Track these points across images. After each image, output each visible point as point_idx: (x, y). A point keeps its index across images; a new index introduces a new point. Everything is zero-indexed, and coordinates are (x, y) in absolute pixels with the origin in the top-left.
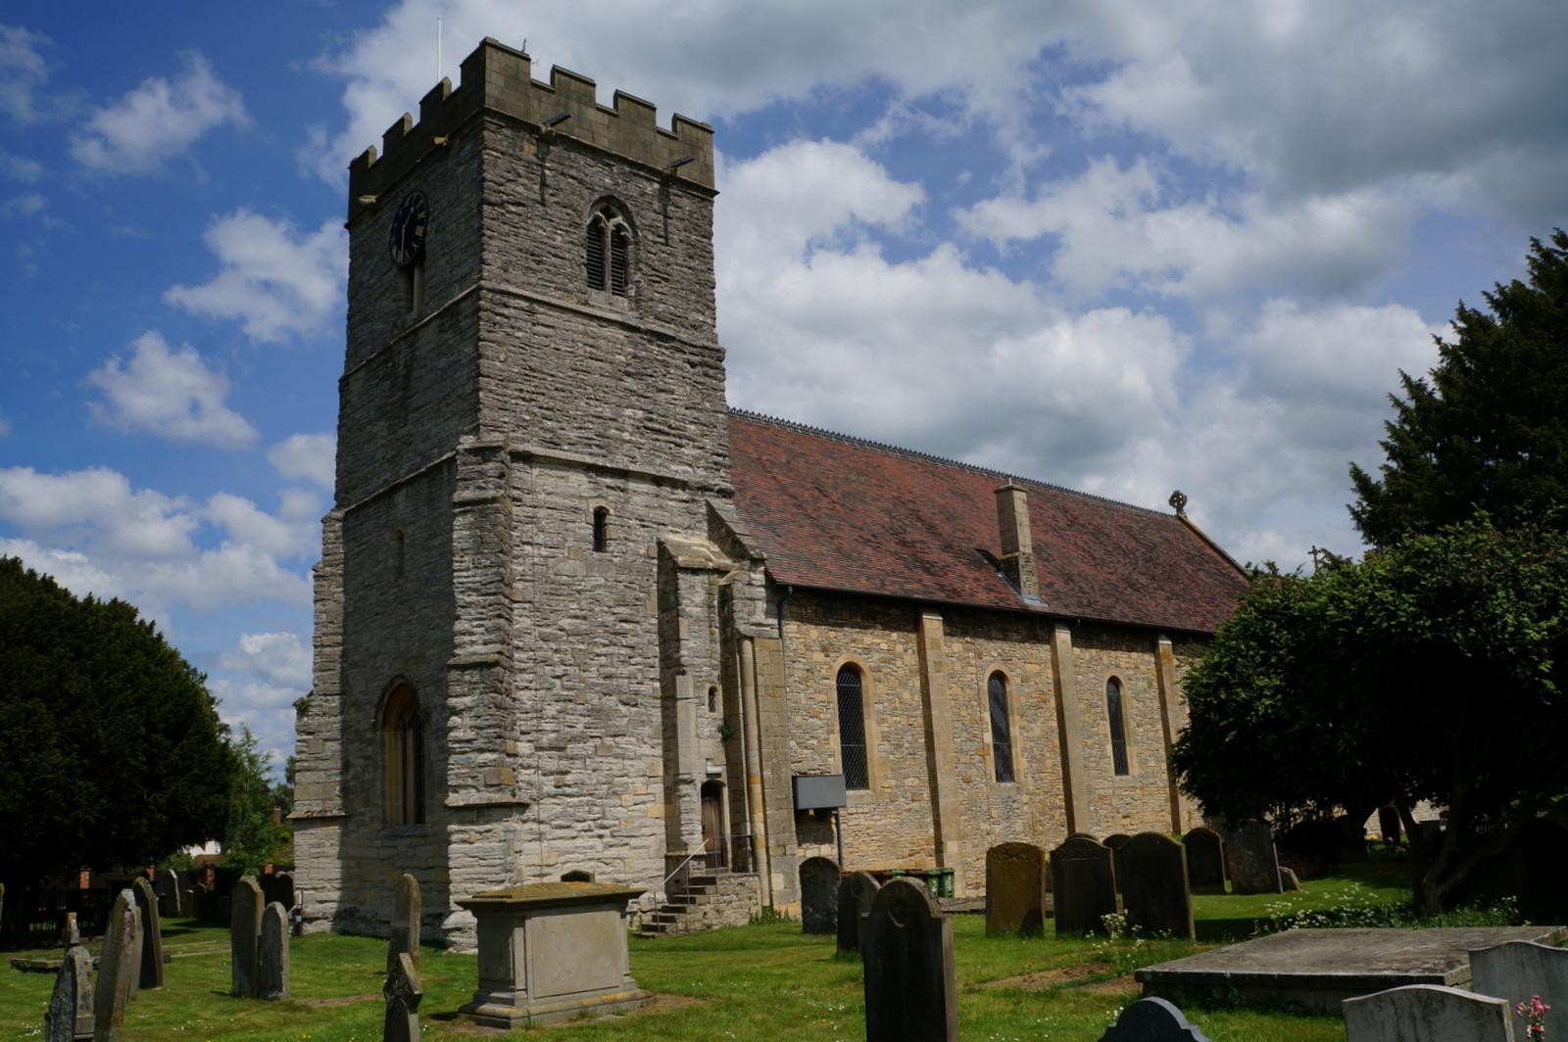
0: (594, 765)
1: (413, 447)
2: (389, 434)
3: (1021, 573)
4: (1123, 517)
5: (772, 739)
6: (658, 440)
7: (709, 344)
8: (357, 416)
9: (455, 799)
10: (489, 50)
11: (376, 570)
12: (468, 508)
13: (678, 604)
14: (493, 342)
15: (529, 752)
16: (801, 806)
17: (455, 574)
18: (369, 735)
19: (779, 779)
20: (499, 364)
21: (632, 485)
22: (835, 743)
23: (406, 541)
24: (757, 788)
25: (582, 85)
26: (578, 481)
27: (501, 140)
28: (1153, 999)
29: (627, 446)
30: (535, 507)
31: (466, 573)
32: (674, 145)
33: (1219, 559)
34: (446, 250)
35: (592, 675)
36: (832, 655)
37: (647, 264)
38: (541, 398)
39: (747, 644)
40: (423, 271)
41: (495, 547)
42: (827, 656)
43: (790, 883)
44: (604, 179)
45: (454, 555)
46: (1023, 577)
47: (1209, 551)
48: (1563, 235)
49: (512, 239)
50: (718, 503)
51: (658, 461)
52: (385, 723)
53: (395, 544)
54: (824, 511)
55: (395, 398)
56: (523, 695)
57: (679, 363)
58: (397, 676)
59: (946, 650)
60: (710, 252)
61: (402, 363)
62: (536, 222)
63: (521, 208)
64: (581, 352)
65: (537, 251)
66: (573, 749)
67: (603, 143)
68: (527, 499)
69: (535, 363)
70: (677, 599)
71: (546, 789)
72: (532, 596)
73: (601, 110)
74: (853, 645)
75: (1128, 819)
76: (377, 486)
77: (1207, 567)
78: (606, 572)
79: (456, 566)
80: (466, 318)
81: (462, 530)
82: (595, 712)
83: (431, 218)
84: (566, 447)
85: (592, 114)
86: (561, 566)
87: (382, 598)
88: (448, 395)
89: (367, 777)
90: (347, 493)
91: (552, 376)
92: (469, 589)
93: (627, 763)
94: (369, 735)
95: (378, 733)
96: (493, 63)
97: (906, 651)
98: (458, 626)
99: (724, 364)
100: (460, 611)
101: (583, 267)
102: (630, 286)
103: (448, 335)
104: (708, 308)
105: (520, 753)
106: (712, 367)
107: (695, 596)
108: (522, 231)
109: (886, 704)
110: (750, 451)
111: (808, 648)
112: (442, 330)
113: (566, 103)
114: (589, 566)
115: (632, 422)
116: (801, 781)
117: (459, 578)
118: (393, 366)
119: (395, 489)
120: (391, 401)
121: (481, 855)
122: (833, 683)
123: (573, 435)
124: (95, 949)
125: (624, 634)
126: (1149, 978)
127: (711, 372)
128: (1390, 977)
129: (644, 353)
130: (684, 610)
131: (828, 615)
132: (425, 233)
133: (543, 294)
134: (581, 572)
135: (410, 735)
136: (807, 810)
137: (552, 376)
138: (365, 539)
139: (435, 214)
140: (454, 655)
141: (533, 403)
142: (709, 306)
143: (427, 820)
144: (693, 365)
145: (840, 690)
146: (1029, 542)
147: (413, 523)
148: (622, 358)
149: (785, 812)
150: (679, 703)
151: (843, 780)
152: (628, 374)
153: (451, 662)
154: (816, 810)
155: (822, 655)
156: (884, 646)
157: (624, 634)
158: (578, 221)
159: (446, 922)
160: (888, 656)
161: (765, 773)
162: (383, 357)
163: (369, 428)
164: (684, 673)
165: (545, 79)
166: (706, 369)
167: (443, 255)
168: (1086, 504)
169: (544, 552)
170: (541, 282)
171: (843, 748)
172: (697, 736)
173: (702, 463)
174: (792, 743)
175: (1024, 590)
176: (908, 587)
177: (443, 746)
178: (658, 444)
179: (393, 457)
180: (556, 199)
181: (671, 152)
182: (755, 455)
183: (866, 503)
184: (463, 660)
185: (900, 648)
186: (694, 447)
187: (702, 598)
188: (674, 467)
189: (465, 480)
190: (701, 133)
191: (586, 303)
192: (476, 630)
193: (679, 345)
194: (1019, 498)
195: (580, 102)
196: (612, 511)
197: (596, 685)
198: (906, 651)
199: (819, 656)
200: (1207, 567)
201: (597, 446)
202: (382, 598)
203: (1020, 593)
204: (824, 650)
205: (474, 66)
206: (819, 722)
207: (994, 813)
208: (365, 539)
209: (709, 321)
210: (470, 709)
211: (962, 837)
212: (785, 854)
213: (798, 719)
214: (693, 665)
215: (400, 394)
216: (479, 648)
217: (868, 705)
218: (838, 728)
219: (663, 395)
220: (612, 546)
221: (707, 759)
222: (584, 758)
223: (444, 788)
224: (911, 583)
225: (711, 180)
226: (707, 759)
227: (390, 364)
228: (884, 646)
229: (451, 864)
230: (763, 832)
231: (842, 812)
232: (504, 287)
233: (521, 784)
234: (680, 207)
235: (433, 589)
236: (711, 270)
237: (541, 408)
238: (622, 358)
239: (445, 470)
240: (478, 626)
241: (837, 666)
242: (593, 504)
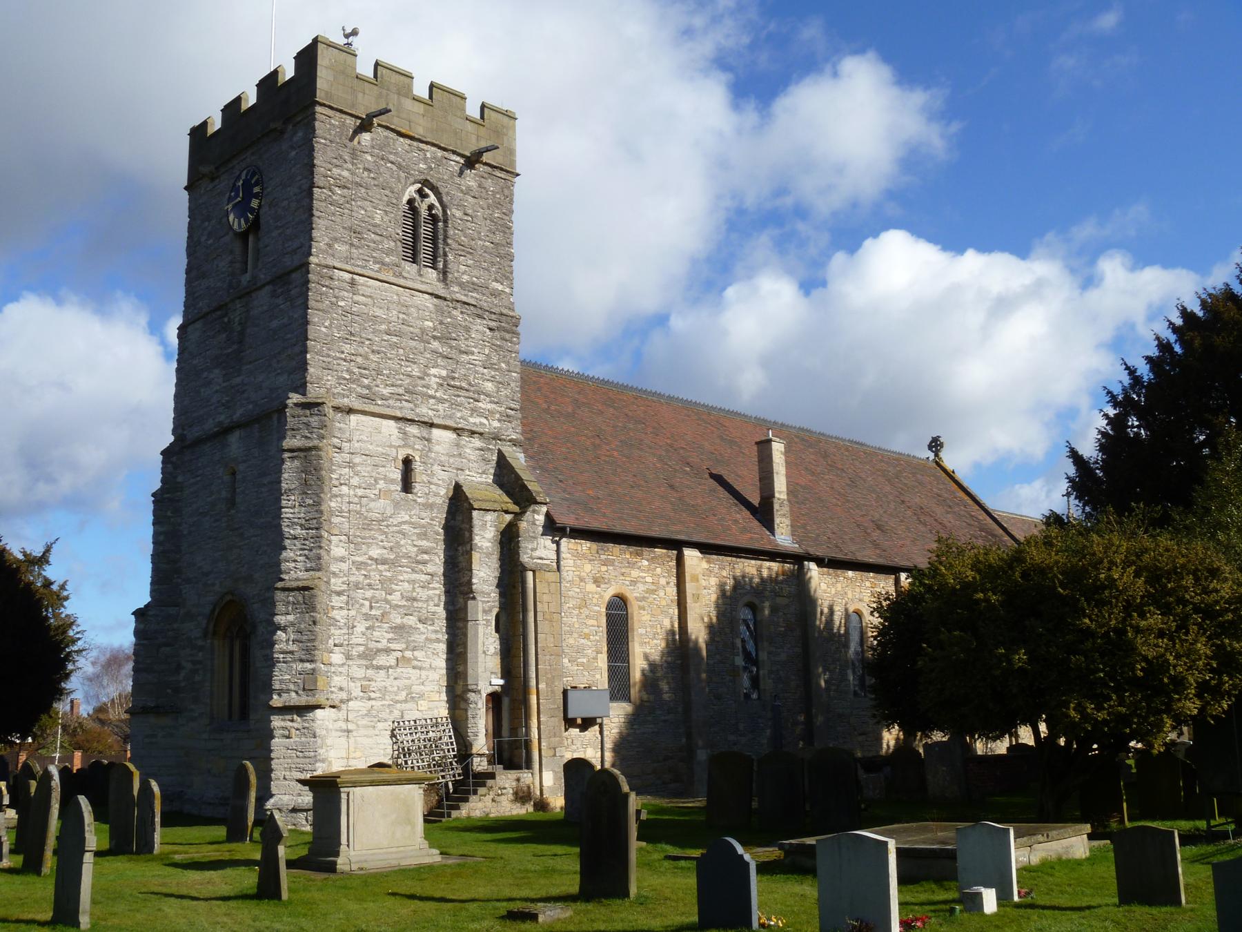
0: (395, 675)
1: (245, 395)
2: (224, 382)
3: (775, 516)
4: (882, 461)
5: (548, 657)
6: (459, 396)
8: (194, 362)
9: (276, 701)
10: (320, 46)
11: (209, 499)
12: (295, 454)
13: (471, 539)
14: (319, 310)
15: (341, 663)
16: (570, 715)
17: (283, 510)
18: (200, 643)
19: (553, 692)
20: (324, 329)
21: (435, 432)
22: (603, 662)
23: (239, 477)
24: (533, 699)
25: (402, 78)
27: (330, 129)
28: (727, 838)
29: (432, 401)
30: (352, 454)
31: (291, 510)
32: (482, 130)
33: (970, 502)
34: (279, 224)
35: (395, 598)
36: (602, 586)
37: (454, 240)
38: (359, 359)
39: (530, 575)
40: (258, 239)
41: (313, 480)
42: (598, 586)
43: (555, 779)
44: (422, 160)
45: (282, 495)
46: (777, 520)
47: (961, 494)
49: (338, 219)
50: (508, 450)
51: (459, 415)
52: (214, 633)
53: (227, 478)
54: (603, 458)
55: (230, 350)
56: (335, 614)
57: (480, 328)
58: (227, 593)
59: (704, 583)
60: (510, 228)
61: (237, 319)
62: (359, 203)
63: (345, 190)
64: (395, 319)
65: (359, 229)
66: (382, 660)
67: (419, 131)
68: (346, 446)
69: (356, 328)
70: (471, 535)
71: (354, 694)
72: (347, 530)
73: (416, 99)
74: (622, 578)
75: (864, 736)
76: (210, 426)
77: (957, 509)
78: (411, 510)
79: (284, 503)
80: (296, 287)
81: (290, 473)
82: (399, 630)
83: (265, 192)
84: (379, 402)
85: (408, 104)
86: (372, 505)
87: (214, 525)
88: (279, 353)
89: (197, 678)
90: (184, 430)
91: (369, 340)
92: (297, 524)
93: (424, 673)
95: (209, 641)
96: (324, 58)
97: (668, 583)
98: (284, 554)
99: (519, 329)
100: (287, 542)
101: (399, 244)
102: (439, 259)
103: (280, 301)
104: (507, 278)
105: (333, 663)
106: (508, 332)
107: (485, 534)
108: (346, 211)
109: (648, 630)
110: (541, 401)
111: (582, 580)
112: (274, 295)
113: (388, 95)
114: (397, 505)
115: (437, 380)
116: (571, 694)
117: (287, 513)
118: (229, 322)
119: (227, 430)
120: (225, 352)
121: (300, 748)
123: (386, 391)
124: (664, 686)
125: (425, 563)
126: (787, 847)
127: (508, 336)
128: (935, 849)
129: (449, 320)
130: (476, 544)
131: (600, 552)
132: (260, 206)
133: (363, 267)
134: (389, 511)
136: (575, 719)
137: (369, 340)
138: (200, 472)
139: (269, 190)
140: (283, 580)
141: (352, 364)
142: (506, 276)
143: (251, 718)
145: (608, 616)
146: (784, 488)
147: (244, 462)
148: (431, 324)
149: (557, 719)
150: (470, 623)
151: (608, 696)
152: (435, 338)
153: (279, 585)
154: (583, 719)
155: (594, 586)
156: (649, 579)
157: (425, 563)
158: (395, 201)
159: (268, 803)
160: (654, 588)
161: (540, 686)
162: (219, 313)
163: (205, 374)
164: (474, 598)
165: (368, 72)
166: (503, 334)
167: (277, 228)
168: (847, 450)
169: (360, 492)
170: (361, 256)
171: (609, 666)
172: (484, 652)
173: (497, 416)
174: (566, 661)
175: (778, 531)
176: (673, 528)
177: (267, 655)
178: (459, 399)
179: (228, 402)
180: (376, 183)
181: (478, 138)
182: (545, 406)
183: (641, 450)
184: (288, 585)
185: (663, 581)
186: (491, 402)
187: (492, 534)
188: (472, 420)
189: (293, 430)
190: (506, 119)
191: (400, 276)
192: (299, 559)
193: (480, 312)
194: (778, 448)
195: (399, 94)
196: (417, 458)
197: (400, 606)
198: (668, 583)
199: (591, 587)
200: (957, 509)
201: (406, 401)
202: (214, 525)
203: (774, 535)
204: (597, 581)
205: (307, 58)
206: (589, 643)
207: (741, 726)
208: (200, 472)
209: (507, 290)
210: (293, 624)
212: (555, 755)
213: (571, 641)
214: (483, 592)
215: (235, 347)
216: (301, 574)
217: (633, 629)
218: (605, 649)
219: (465, 356)
220: (417, 487)
221: (492, 673)
222: (387, 668)
223: (268, 689)
224: (674, 524)
225: (513, 163)
226: (492, 673)
227: (226, 320)
228: (649, 579)
229: (273, 755)
230: (537, 737)
231: (606, 721)
233: (333, 689)
234: (485, 188)
235: (262, 520)
236: (510, 244)
237: (359, 368)
238: (431, 324)
239: (275, 417)
240: (300, 555)
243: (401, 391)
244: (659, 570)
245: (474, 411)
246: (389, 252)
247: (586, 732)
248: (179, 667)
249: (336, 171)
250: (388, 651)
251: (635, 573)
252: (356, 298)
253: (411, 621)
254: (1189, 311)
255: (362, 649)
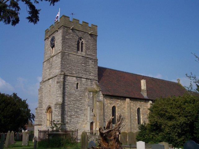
7: (95, 59)
18: (45, 114)
21: (83, 79)
26: (75, 78)
48: (59, 145)
66: (73, 117)
82: (77, 112)
94: (45, 114)
111: (107, 103)
114: (76, 91)
122: (111, 109)
135: (51, 114)
144: (93, 62)
169: (70, 89)
199: (109, 105)
204: (110, 104)
211: (136, 119)
225: (97, 34)
232: (65, 51)
241: (112, 106)
242: (76, 82)
243: (77, 72)
244: (122, 102)
245: (90, 75)
246: (75, 50)
247: (32, 107)
248: (42, 118)
249: (66, 37)
250: (74, 115)
251: (117, 102)
252: (69, 57)
253: (78, 110)
254: (2, 94)
255: (69, 115)
